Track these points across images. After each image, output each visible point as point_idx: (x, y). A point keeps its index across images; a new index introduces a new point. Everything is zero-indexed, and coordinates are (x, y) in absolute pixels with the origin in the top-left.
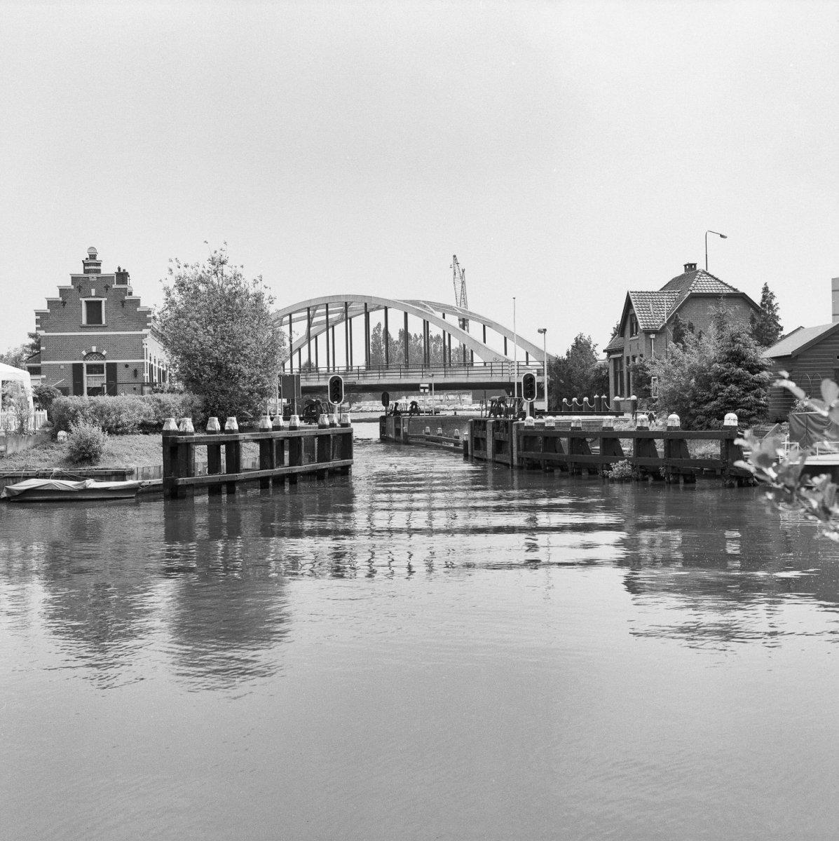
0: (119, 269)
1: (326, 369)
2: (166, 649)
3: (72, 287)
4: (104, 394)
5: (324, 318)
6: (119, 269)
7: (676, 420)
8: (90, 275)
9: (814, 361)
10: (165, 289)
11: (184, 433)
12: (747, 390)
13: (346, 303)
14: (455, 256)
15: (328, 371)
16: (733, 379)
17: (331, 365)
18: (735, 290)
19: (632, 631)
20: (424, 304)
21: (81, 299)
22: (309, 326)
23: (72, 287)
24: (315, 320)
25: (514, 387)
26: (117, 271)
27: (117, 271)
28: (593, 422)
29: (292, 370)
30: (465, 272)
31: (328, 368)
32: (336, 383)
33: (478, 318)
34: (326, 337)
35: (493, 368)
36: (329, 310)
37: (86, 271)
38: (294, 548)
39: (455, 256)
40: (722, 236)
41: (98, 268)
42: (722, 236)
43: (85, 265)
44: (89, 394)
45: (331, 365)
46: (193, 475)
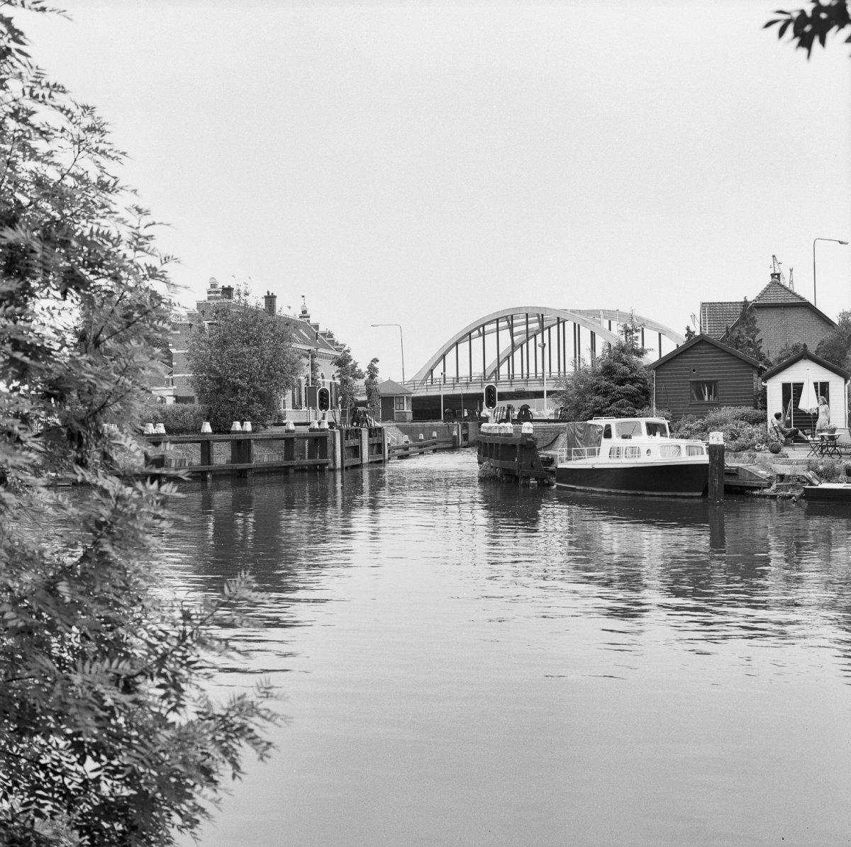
0: (268, 292)
1: (557, 374)
2: (841, 654)
3: (197, 312)
4: (444, 396)
5: (524, 328)
6: (268, 292)
7: (509, 428)
8: (211, 302)
9: (671, 374)
10: (773, 275)
11: (245, 432)
12: (612, 402)
13: (527, 314)
14: (774, 256)
15: (522, 377)
16: (603, 390)
17: (562, 370)
18: (802, 299)
19: (378, 577)
20: (595, 314)
21: (204, 322)
22: (512, 335)
23: (197, 312)
24: (516, 330)
25: (483, 398)
26: (266, 294)
27: (266, 294)
28: (549, 429)
29: (471, 378)
30: (793, 272)
31: (522, 375)
32: (490, 391)
33: (654, 326)
34: (468, 346)
35: (413, 385)
36: (529, 319)
37: (209, 298)
38: (676, 539)
39: (774, 256)
40: (841, 243)
41: (209, 295)
42: (841, 243)
43: (209, 292)
44: (543, 392)
45: (562, 370)
46: (250, 462)
